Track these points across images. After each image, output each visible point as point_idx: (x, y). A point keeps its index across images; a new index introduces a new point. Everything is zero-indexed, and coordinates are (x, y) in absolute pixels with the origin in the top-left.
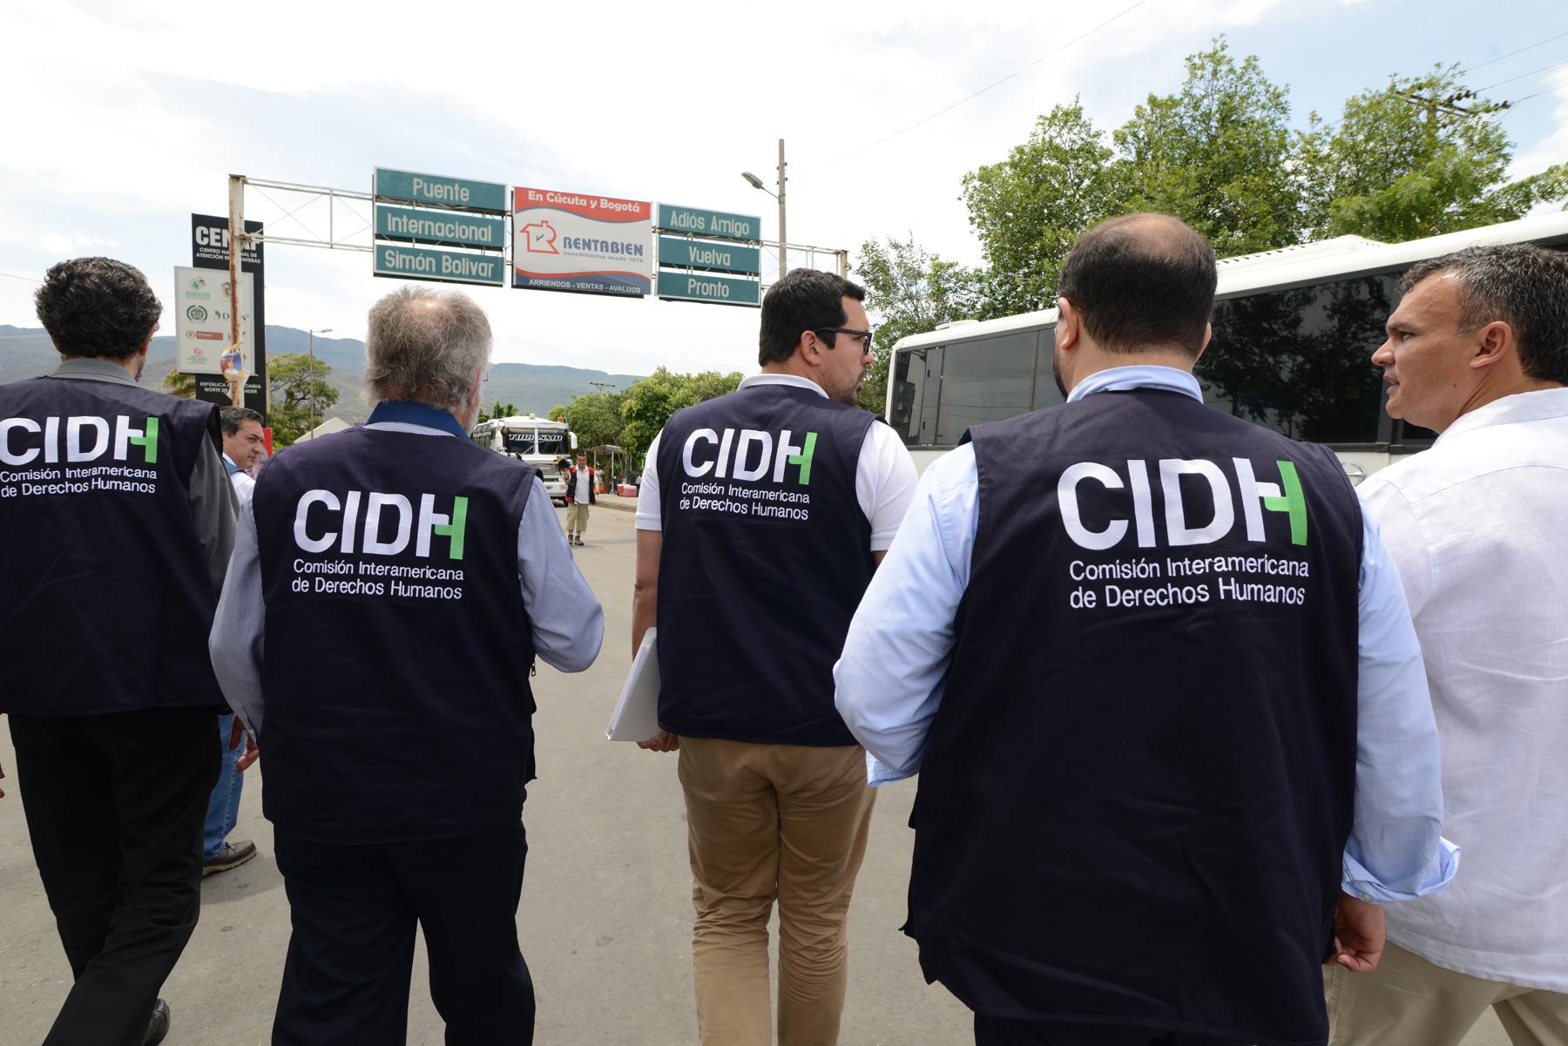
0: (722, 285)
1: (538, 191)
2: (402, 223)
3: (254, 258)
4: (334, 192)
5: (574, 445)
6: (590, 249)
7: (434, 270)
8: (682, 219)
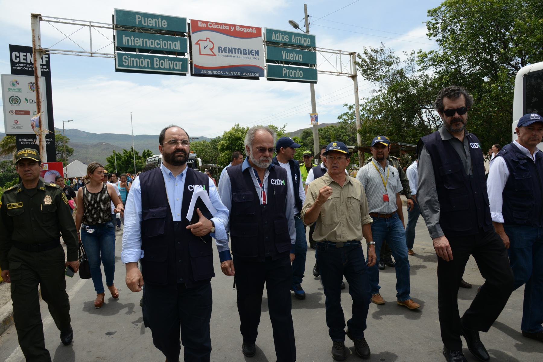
0: (299, 71)
1: (203, 22)
2: (131, 40)
3: (45, 68)
4: (92, 24)
5: (200, 164)
6: (232, 53)
7: (150, 66)
8: (278, 36)
